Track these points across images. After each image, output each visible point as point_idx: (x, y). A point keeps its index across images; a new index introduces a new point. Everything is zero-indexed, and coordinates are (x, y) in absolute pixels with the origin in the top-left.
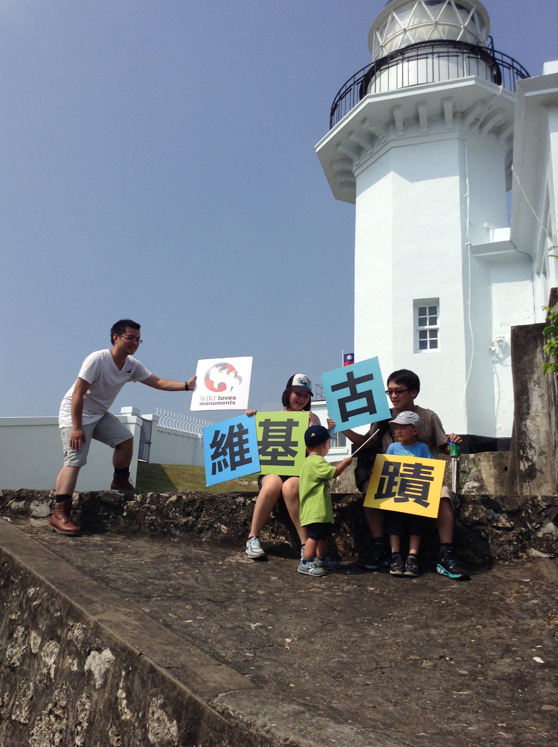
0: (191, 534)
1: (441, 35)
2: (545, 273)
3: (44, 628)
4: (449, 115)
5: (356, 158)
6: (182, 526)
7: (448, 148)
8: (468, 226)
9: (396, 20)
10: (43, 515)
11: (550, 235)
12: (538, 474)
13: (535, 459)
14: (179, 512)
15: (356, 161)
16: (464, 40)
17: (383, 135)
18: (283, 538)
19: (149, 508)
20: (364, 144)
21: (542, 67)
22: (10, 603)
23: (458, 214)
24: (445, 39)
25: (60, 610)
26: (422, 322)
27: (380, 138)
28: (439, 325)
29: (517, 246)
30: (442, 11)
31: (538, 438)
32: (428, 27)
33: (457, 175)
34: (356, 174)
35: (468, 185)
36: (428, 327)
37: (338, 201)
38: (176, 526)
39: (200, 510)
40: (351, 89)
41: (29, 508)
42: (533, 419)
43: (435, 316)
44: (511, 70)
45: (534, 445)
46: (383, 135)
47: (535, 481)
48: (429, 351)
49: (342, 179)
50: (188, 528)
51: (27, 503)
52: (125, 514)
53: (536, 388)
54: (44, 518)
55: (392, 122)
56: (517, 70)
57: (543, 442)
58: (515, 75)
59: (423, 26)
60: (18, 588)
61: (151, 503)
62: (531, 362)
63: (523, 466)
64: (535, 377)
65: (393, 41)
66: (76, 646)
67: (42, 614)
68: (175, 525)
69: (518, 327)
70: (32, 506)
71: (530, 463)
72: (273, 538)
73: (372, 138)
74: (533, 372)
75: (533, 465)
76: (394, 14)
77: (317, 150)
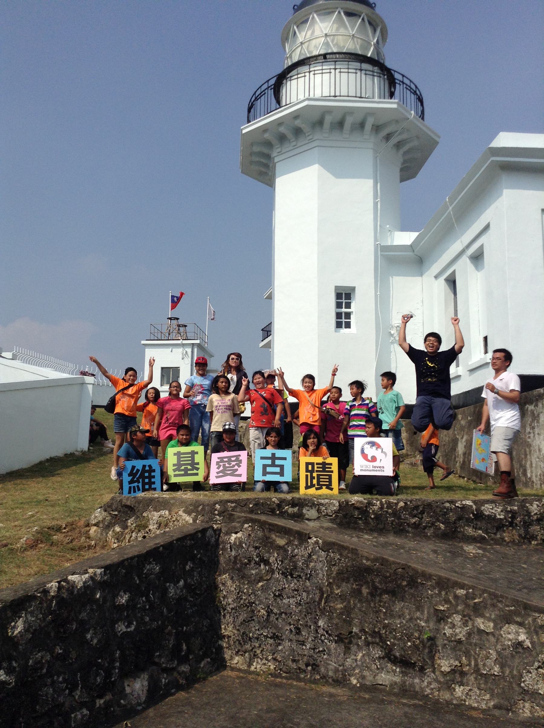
0: (419, 530)
1: (356, 47)
2: (452, 282)
5: (278, 146)
6: (412, 524)
7: (365, 152)
8: (378, 228)
9: (316, 20)
10: (313, 518)
11: (477, 258)
14: (409, 515)
16: (373, 57)
17: (310, 133)
19: (387, 512)
20: (289, 135)
22: (428, 598)
23: (372, 216)
24: (360, 53)
25: (514, 606)
26: (339, 305)
27: (307, 135)
30: (358, 23)
32: (345, 37)
33: (368, 178)
34: (276, 160)
35: (379, 192)
36: (344, 310)
38: (408, 525)
39: (422, 512)
41: (303, 513)
43: (349, 301)
46: (310, 133)
48: (344, 331)
50: (416, 526)
52: (373, 516)
54: (315, 520)
56: (407, 85)
58: (405, 89)
59: (342, 35)
61: (387, 508)
65: (311, 42)
67: (485, 608)
70: (304, 511)
72: (475, 532)
73: (298, 132)
76: (315, 15)
77: (244, 132)
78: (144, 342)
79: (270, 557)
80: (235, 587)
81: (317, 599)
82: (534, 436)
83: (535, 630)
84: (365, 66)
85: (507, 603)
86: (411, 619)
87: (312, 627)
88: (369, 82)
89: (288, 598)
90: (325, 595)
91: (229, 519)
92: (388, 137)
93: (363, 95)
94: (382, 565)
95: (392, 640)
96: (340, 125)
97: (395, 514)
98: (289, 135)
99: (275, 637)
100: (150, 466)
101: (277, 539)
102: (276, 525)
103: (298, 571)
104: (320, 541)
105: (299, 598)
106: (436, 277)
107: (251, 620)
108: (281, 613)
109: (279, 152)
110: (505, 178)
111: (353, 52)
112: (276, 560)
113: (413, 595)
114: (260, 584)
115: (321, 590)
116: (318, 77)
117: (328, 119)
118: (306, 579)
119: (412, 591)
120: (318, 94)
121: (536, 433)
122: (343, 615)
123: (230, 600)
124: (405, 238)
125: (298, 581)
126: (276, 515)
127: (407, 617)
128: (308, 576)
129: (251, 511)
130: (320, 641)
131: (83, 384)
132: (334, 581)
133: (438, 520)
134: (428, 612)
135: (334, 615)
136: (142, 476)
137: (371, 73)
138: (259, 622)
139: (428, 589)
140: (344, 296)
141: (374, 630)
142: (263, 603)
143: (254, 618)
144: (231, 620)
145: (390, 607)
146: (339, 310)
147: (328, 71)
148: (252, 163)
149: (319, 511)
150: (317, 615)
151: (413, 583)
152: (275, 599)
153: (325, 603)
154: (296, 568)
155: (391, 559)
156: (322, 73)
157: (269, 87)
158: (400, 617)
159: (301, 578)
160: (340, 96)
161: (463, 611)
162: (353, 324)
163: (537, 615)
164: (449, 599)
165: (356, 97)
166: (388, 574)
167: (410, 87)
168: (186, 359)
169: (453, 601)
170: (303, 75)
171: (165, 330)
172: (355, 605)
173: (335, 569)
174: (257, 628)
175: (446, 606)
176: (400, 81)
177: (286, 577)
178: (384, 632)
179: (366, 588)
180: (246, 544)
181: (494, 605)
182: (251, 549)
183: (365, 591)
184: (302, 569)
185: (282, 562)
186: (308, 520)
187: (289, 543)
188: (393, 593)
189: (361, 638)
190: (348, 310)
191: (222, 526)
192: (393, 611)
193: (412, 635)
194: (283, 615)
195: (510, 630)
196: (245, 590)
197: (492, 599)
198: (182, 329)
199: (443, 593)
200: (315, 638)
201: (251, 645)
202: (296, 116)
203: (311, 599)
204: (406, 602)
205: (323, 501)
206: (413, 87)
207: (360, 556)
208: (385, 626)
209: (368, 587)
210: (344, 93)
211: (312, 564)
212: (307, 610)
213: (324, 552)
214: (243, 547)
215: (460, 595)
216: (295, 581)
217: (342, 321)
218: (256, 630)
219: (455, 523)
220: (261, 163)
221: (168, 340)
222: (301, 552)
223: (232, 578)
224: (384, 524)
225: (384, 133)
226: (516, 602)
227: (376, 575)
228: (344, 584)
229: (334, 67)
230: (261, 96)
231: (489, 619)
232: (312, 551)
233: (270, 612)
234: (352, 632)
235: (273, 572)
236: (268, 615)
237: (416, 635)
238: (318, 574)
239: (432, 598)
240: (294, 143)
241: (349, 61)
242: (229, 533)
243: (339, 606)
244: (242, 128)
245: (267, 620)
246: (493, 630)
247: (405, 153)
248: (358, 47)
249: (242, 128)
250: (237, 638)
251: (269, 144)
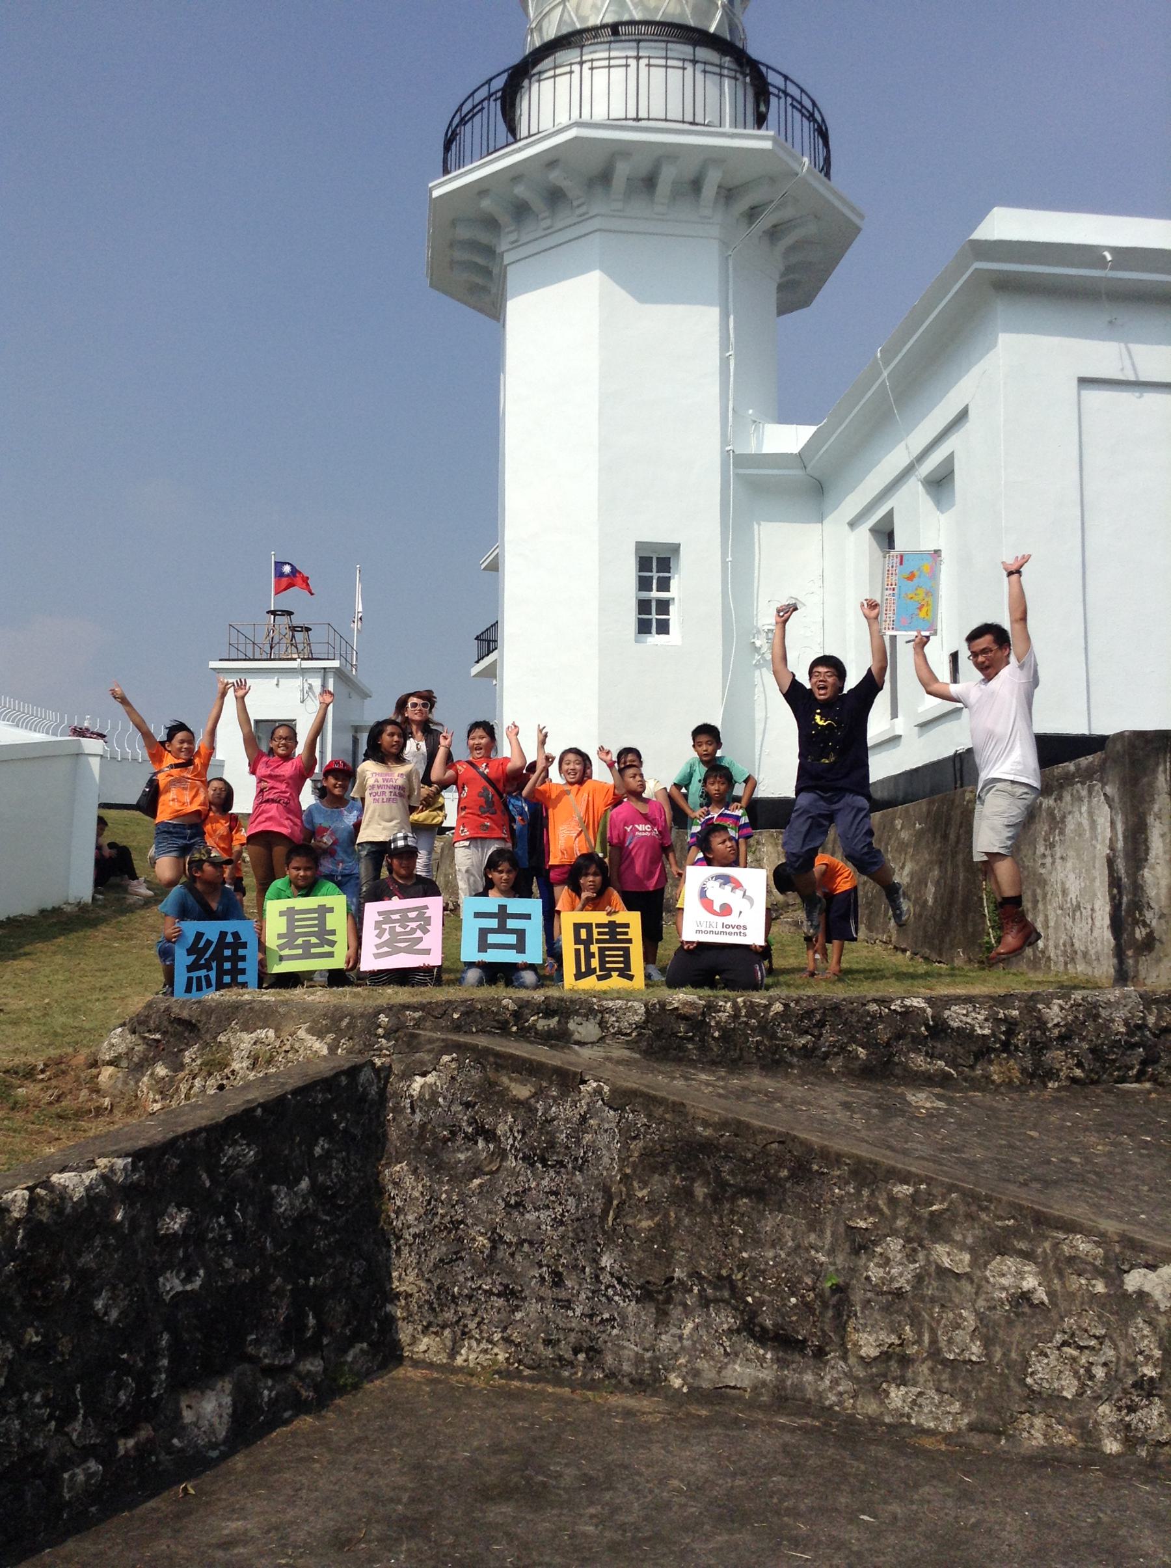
1: (683, 10)
3: (969, 1241)
4: (709, 190)
5: (512, 228)
6: (800, 1049)
7: (700, 247)
11: (941, 483)
12: (1157, 944)
13: (1154, 923)
14: (793, 1029)
15: (511, 232)
18: (941, 1063)
19: (746, 1023)
20: (537, 204)
22: (833, 1203)
23: (716, 390)
24: (692, 23)
25: (1013, 1217)
26: (644, 584)
27: (575, 203)
28: (674, 592)
31: (1158, 894)
33: (711, 304)
36: (655, 594)
37: (436, 293)
39: (821, 1024)
40: (483, 108)
42: (1152, 868)
43: (667, 575)
44: (782, 101)
45: (1153, 904)
47: (1154, 955)
48: (654, 639)
49: (460, 255)
50: (807, 1053)
51: (563, 1021)
52: (716, 1034)
53: (1157, 824)
54: (593, 1043)
56: (793, 98)
57: (1164, 901)
58: (789, 108)
60: (849, 1183)
61: (748, 1015)
62: (1151, 785)
63: (1140, 933)
64: (1156, 808)
66: (1093, 1265)
67: (954, 1222)
68: (789, 1049)
69: (1135, 732)
70: (571, 1025)
71: (1148, 930)
73: (555, 197)
74: (1153, 801)
75: (1152, 932)
78: (214, 664)
79: (496, 1125)
80: (421, 1189)
81: (599, 1211)
82: (1053, 863)
83: (1056, 1266)
84: (703, 53)
85: (1000, 1212)
86: (798, 1246)
87: (587, 1269)
88: (712, 91)
89: (537, 1209)
90: (615, 1202)
91: (409, 1044)
92: (752, 214)
93: (699, 119)
94: (736, 1135)
95: (757, 1294)
97: (765, 1028)
98: (537, 204)
99: (508, 1293)
100: (236, 935)
101: (513, 1085)
102: (511, 1056)
103: (558, 1153)
104: (606, 1089)
105: (559, 1209)
106: (852, 524)
107: (457, 1259)
108: (521, 1243)
109: (513, 242)
110: (1002, 309)
111: (676, 20)
112: (511, 1130)
113: (801, 1197)
114: (477, 1182)
115: (606, 1191)
116: (601, 75)
117: (622, 170)
118: (574, 1168)
119: (799, 1190)
120: (600, 115)
121: (1058, 855)
122: (653, 1243)
123: (411, 1218)
124: (788, 439)
125: (558, 1173)
126: (511, 1034)
127: (790, 1244)
128: (580, 1161)
129: (457, 1028)
130: (603, 1299)
131: (79, 755)
132: (634, 1170)
133: (853, 1039)
134: (833, 1233)
135: (635, 1242)
136: (218, 956)
137: (717, 70)
138: (473, 1263)
139: (835, 1184)
140: (655, 565)
141: (719, 1274)
142: (482, 1222)
143: (463, 1254)
144: (413, 1259)
145: (753, 1224)
147: (623, 62)
148: (453, 263)
149: (602, 1024)
150: (599, 1245)
151: (801, 1172)
152: (508, 1213)
153: (615, 1219)
154: (553, 1147)
155: (756, 1123)
156: (609, 67)
157: (490, 96)
158: (773, 1246)
159: (565, 1167)
160: (649, 119)
161: (907, 1230)
163: (1062, 1236)
164: (877, 1205)
165: (683, 122)
166: (749, 1155)
167: (800, 103)
168: (309, 702)
169: (886, 1210)
170: (567, 69)
171: (261, 638)
172: (679, 1220)
173: (636, 1146)
174: (469, 1275)
175: (871, 1220)
176: (779, 90)
177: (532, 1165)
178: (739, 1276)
179: (702, 1186)
180: (445, 1098)
181: (971, 1217)
182: (456, 1108)
183: (700, 1191)
184: (567, 1148)
185: (523, 1133)
186: (581, 1044)
187: (538, 1094)
188: (759, 1195)
189: (691, 1290)
190: (645, 595)
191: (392, 1060)
192: (758, 1232)
193: (800, 1280)
194: (526, 1245)
195: (1005, 1268)
196: (444, 1196)
197: (968, 1204)
198: (299, 636)
199: (865, 1193)
200: (593, 1292)
201: (456, 1312)
202: (551, 160)
203: (586, 1209)
204: (786, 1213)
205: (610, 1004)
206: (807, 103)
207: (690, 1118)
208: (743, 1265)
209: (707, 1184)
210: (657, 111)
211: (588, 1138)
212: (577, 1234)
213: (615, 1110)
214: (438, 1105)
215: (900, 1195)
216: (552, 1173)
217: (652, 618)
218: (466, 1279)
219: (888, 1044)
220: (474, 265)
221: (270, 660)
222: (565, 1112)
223: (415, 1171)
224: (741, 1050)
225: (743, 204)
226: (1017, 1210)
227: (724, 1157)
228: (656, 1177)
229: (634, 54)
230: (474, 116)
231: (962, 1247)
232: (589, 1110)
233: (496, 1241)
234: (673, 1278)
235: (503, 1154)
236: (494, 1248)
237: (808, 1281)
238: (600, 1158)
239: (842, 1202)
240: (548, 222)
241: (668, 42)
242: (408, 1075)
243: (645, 1224)
244: (430, 185)
245: (491, 1258)
246: (969, 1270)
247: (792, 249)
248: (688, 11)
249: (430, 185)
250: (427, 1297)
251: (491, 224)
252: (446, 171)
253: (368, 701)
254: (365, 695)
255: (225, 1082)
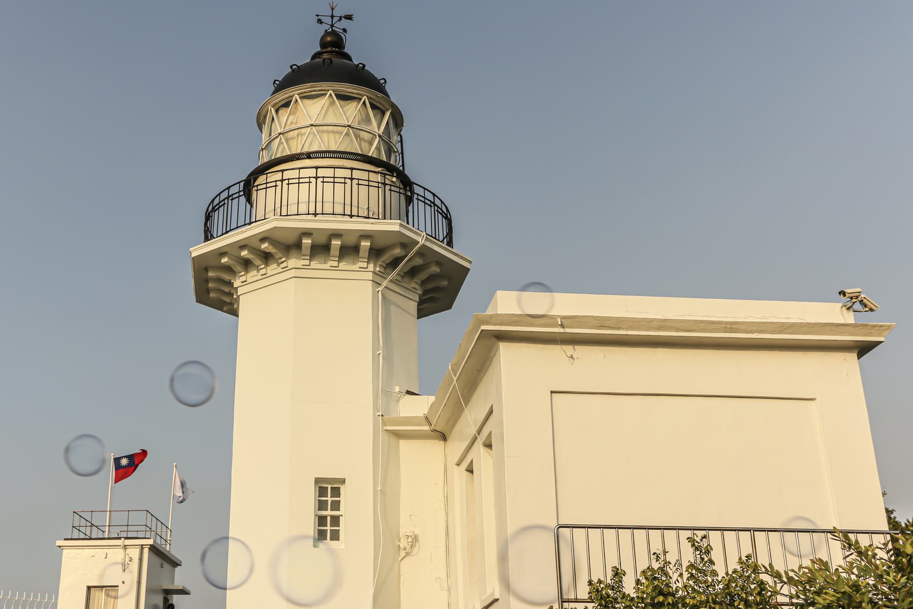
4: (364, 252)
11: (489, 446)
21: (492, 295)
26: (322, 505)
29: (408, 396)
34: (240, 291)
36: (329, 512)
43: (338, 499)
46: (284, 259)
55: (298, 246)
78: (59, 543)
93: (371, 215)
96: (321, 249)
124: (418, 407)
140: (328, 491)
146: (324, 513)
157: (229, 196)
162: (342, 535)
206: (429, 196)
217: (327, 527)
220: (215, 288)
225: (387, 257)
247: (423, 283)
251: (228, 269)
252: (207, 239)
253: (178, 569)
254: (175, 564)
255: (656, 583)
